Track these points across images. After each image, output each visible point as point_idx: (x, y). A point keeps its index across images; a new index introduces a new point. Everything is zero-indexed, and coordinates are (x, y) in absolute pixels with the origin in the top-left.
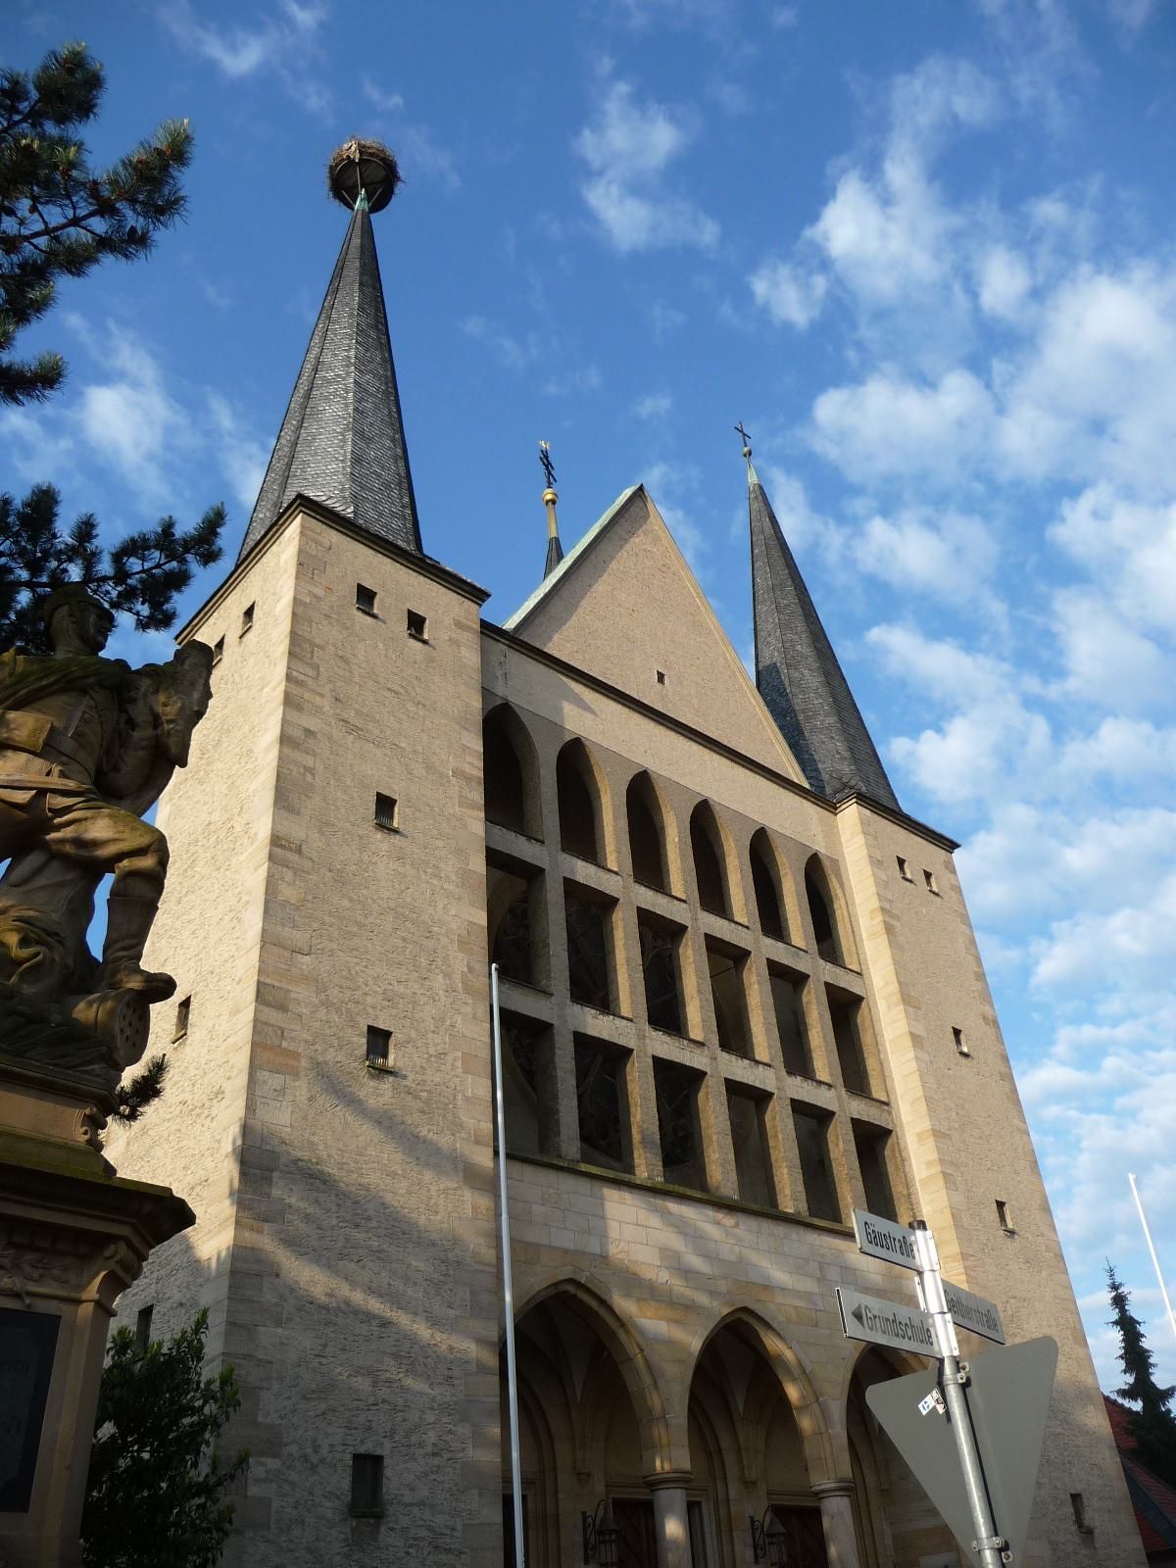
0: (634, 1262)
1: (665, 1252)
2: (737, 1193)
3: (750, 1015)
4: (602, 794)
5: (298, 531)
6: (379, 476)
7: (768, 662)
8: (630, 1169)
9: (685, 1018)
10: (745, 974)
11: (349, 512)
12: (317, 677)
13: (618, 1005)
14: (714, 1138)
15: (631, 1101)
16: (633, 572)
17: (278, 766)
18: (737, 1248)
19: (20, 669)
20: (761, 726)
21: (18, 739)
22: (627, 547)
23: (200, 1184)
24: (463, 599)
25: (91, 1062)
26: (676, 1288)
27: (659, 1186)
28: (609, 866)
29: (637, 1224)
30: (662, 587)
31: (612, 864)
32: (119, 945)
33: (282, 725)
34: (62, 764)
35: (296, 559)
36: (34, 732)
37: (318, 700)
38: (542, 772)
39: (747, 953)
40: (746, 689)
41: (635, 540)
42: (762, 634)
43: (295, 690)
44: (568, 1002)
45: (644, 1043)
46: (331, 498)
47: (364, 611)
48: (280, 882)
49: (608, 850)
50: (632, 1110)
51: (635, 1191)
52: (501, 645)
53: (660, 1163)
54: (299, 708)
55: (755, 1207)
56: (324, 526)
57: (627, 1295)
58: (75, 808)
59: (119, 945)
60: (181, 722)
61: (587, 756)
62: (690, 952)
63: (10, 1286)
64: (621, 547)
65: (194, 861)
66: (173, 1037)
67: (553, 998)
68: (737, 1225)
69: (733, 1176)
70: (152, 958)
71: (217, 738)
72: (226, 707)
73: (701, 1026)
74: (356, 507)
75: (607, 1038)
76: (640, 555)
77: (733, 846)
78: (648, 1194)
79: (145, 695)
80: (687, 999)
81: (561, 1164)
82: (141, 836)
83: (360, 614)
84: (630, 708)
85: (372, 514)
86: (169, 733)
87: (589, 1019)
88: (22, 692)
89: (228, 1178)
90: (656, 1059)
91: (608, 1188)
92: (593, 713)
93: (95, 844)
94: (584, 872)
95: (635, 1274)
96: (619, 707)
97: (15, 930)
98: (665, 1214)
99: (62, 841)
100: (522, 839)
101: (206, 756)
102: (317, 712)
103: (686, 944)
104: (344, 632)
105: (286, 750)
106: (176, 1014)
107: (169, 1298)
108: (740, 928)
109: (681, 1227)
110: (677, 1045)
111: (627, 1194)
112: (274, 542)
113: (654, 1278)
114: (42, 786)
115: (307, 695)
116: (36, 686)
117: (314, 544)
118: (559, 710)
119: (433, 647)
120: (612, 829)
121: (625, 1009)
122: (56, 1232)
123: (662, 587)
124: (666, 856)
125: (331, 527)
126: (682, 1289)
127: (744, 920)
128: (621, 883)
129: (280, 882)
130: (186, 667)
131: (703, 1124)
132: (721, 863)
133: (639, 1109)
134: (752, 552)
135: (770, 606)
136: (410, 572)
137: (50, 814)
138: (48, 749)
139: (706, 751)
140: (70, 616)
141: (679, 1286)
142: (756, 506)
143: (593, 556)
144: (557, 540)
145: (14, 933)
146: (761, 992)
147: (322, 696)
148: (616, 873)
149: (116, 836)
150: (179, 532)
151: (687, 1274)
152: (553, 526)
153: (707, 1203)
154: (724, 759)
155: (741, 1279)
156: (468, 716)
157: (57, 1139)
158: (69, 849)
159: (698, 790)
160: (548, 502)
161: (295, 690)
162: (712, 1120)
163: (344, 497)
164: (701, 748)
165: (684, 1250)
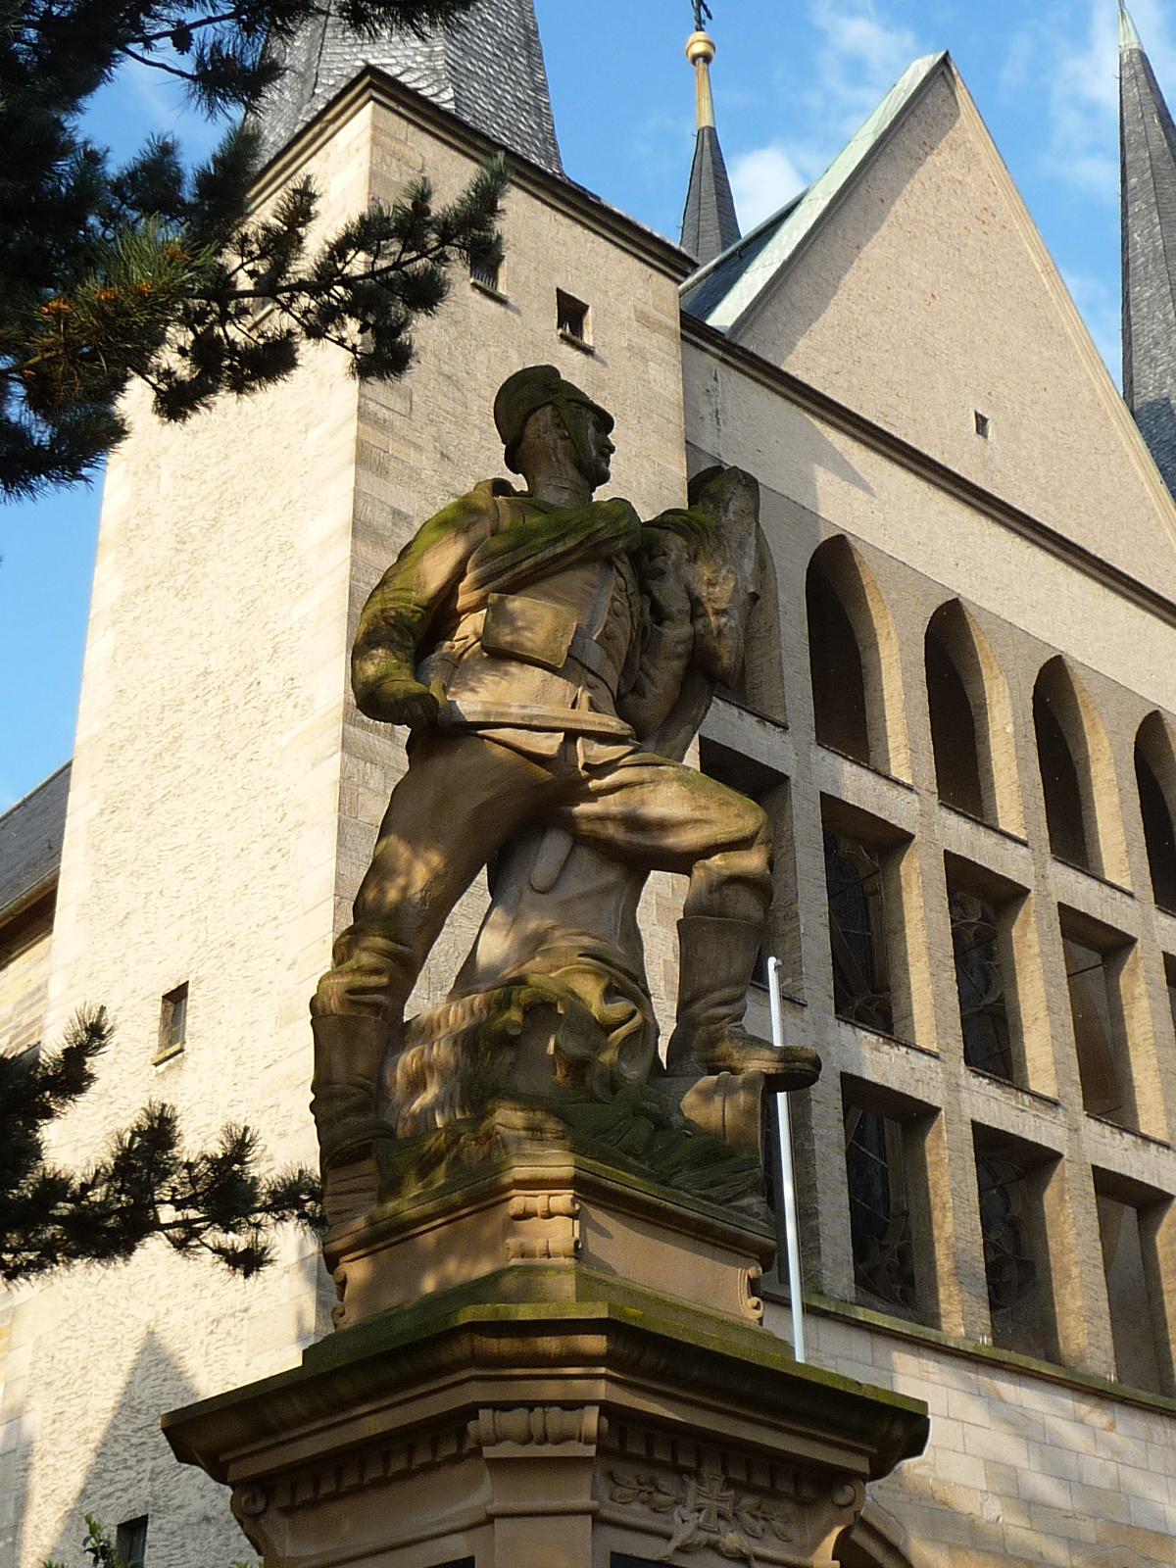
0: (943, 1482)
1: (994, 1467)
2: (1113, 1370)
3: (1132, 1054)
4: (881, 641)
5: (368, 133)
6: (493, 28)
7: (1152, 396)
8: (932, 1319)
9: (1022, 1054)
10: (1123, 980)
11: (446, 99)
12: (408, 415)
13: (910, 1028)
14: (1075, 1271)
15: (935, 1200)
16: (933, 222)
17: (352, 578)
18: (1112, 1467)
19: (506, 522)
20: (1153, 521)
21: (529, 645)
22: (922, 173)
23: (233, 1315)
24: (650, 271)
25: (743, 1194)
26: (1012, 1531)
27: (985, 1353)
28: (894, 774)
29: (948, 1417)
30: (982, 251)
31: (899, 768)
32: (717, 996)
33: (355, 502)
34: (590, 687)
35: (367, 190)
36: (554, 635)
37: (413, 458)
38: (782, 597)
39: (1128, 942)
40: (1128, 449)
41: (934, 160)
42: (1142, 342)
43: (374, 437)
44: (832, 1019)
45: (957, 1099)
46: (409, 69)
47: (483, 291)
48: (361, 790)
49: (891, 745)
50: (937, 1215)
51: (942, 1358)
52: (707, 356)
53: (986, 1313)
54: (382, 471)
55: (1144, 1396)
56: (411, 128)
57: (934, 1540)
58: (621, 763)
59: (717, 996)
60: (736, 613)
61: (854, 567)
62: (1032, 936)
63: (737, 1545)
64: (912, 172)
65: (175, 740)
66: (153, 1054)
67: (806, 1013)
68: (1112, 1427)
69: (1108, 1342)
70: (97, 909)
71: (211, 514)
72: (226, 457)
73: (1053, 1072)
74: (458, 89)
75: (896, 1087)
76: (945, 190)
77: (1106, 743)
78: (964, 1364)
79: (677, 568)
80: (1027, 1021)
81: (825, 1307)
82: (738, 816)
83: (476, 295)
84: (929, 481)
85: (484, 104)
86: (720, 631)
87: (867, 1053)
88: (525, 565)
89: (293, 1310)
90: (976, 1126)
91: (900, 1351)
92: (867, 488)
93: (663, 825)
94: (855, 785)
95: (946, 1504)
96: (911, 479)
97: (589, 972)
98: (993, 1401)
99: (601, 818)
100: (751, 720)
101: (189, 547)
102: (410, 477)
103: (1026, 922)
104: (452, 330)
105: (362, 549)
106: (159, 1012)
107: (180, 1507)
108: (1118, 894)
109: (1020, 1425)
110: (1013, 1103)
111: (931, 1363)
112: (315, 153)
113: (977, 1513)
114: (574, 726)
115: (393, 447)
116: (548, 553)
117: (395, 161)
118: (809, 482)
119: (603, 362)
120: (900, 705)
121: (924, 1033)
122: (777, 1460)
123: (982, 251)
124: (989, 759)
125: (423, 129)
126: (1023, 1533)
127: (1125, 883)
128: (917, 805)
129: (361, 790)
130: (731, 515)
131: (1053, 1245)
132: (1080, 774)
133: (950, 1214)
134: (1124, 181)
135: (1158, 289)
136: (559, 217)
137: (584, 774)
138: (571, 666)
139: (1061, 565)
140: (558, 425)
141: (1017, 1529)
142: (1133, 92)
143: (862, 189)
144: (712, 131)
145: (590, 977)
146: (1153, 1012)
147: (418, 448)
148: (909, 788)
149: (697, 814)
150: (437, 207)
151: (1031, 1506)
152: (705, 105)
153: (1064, 1386)
154: (1090, 582)
155: (1118, 1519)
156: (666, 492)
157: (730, 1317)
158: (612, 831)
159: (1045, 637)
160: (695, 59)
161: (374, 437)
162: (1071, 1238)
163: (434, 70)
164: (1051, 559)
165: (1025, 1464)
